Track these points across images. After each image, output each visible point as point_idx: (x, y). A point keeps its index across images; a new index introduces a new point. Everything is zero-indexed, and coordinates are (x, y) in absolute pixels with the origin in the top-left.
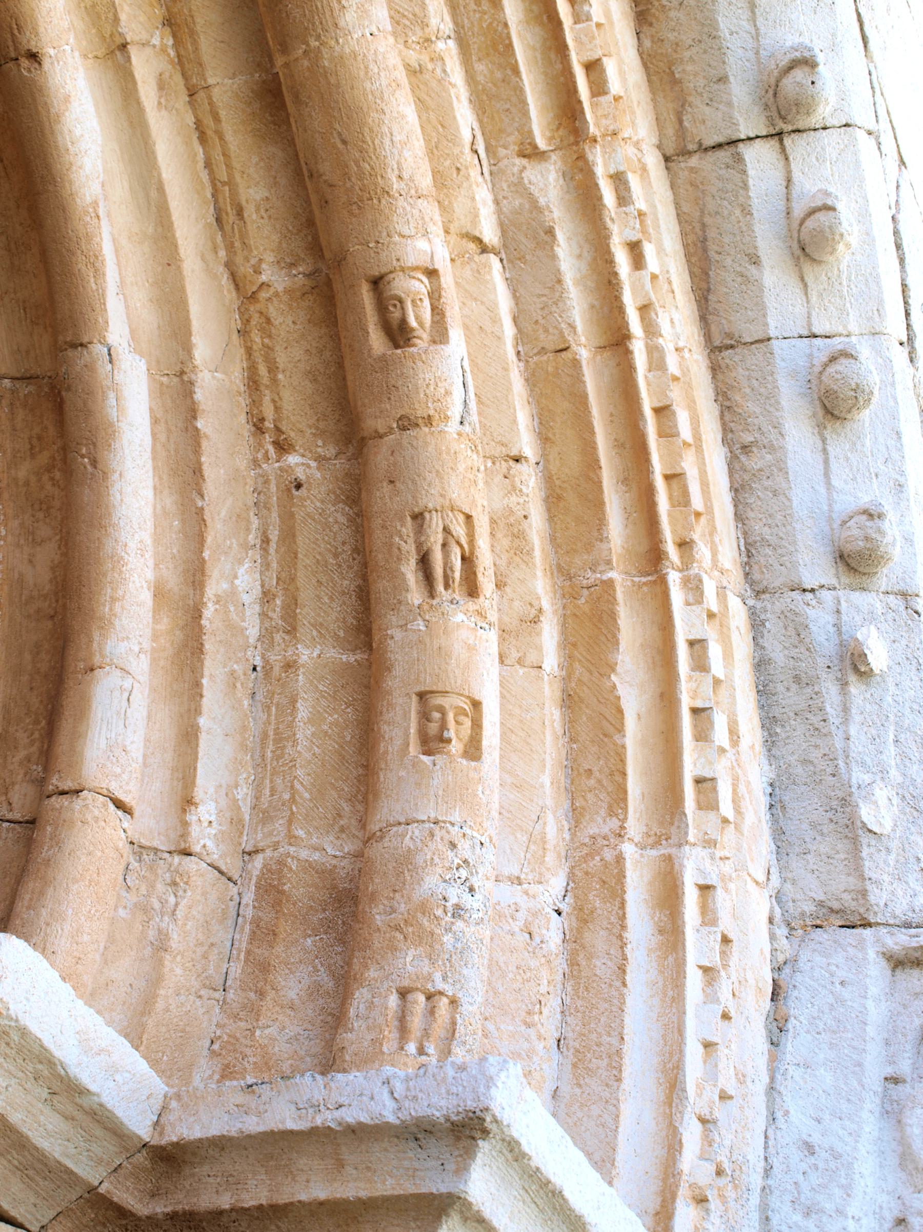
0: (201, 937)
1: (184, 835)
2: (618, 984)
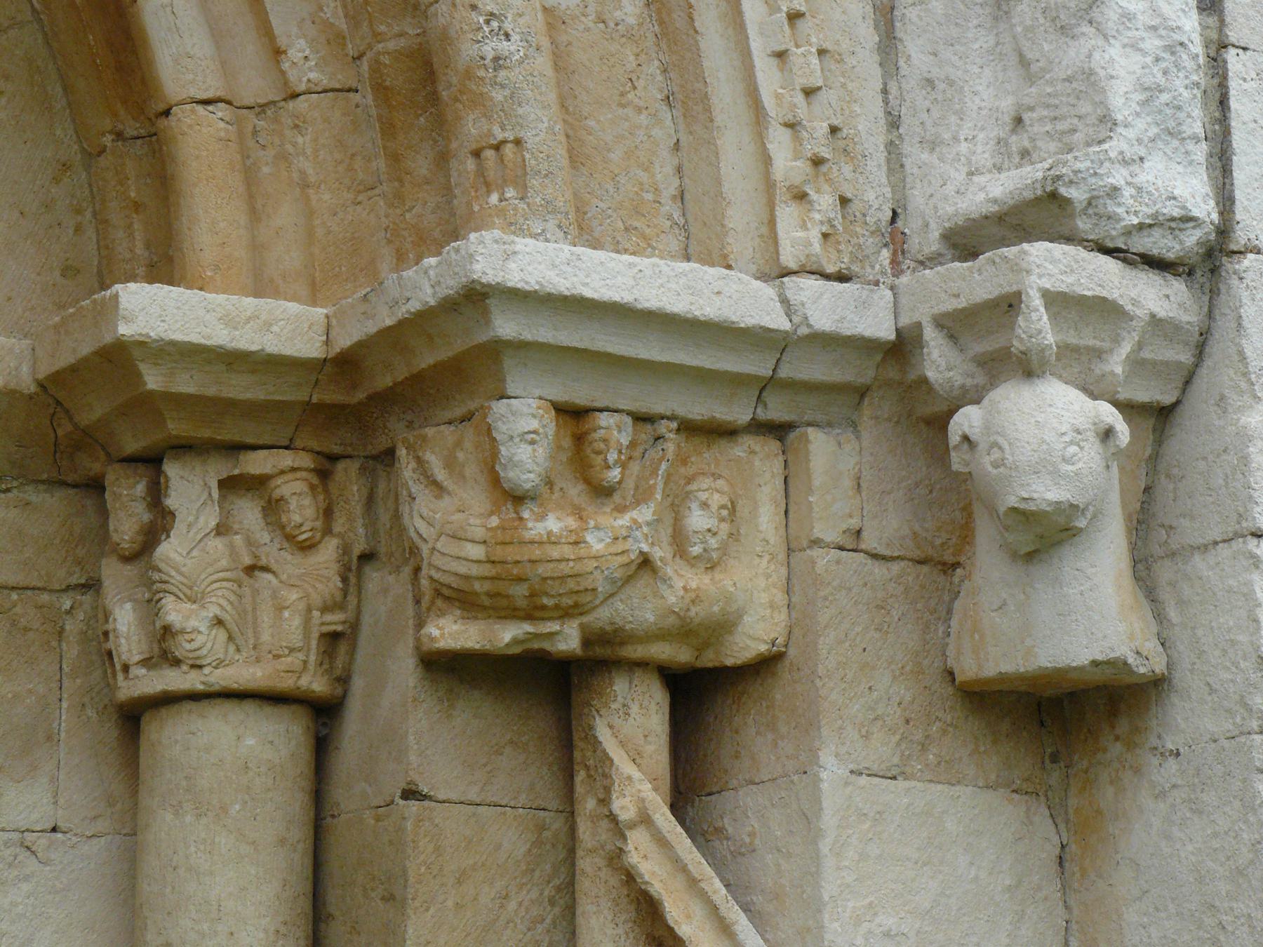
0: (338, 156)
1: (286, 83)
2: (692, 32)
